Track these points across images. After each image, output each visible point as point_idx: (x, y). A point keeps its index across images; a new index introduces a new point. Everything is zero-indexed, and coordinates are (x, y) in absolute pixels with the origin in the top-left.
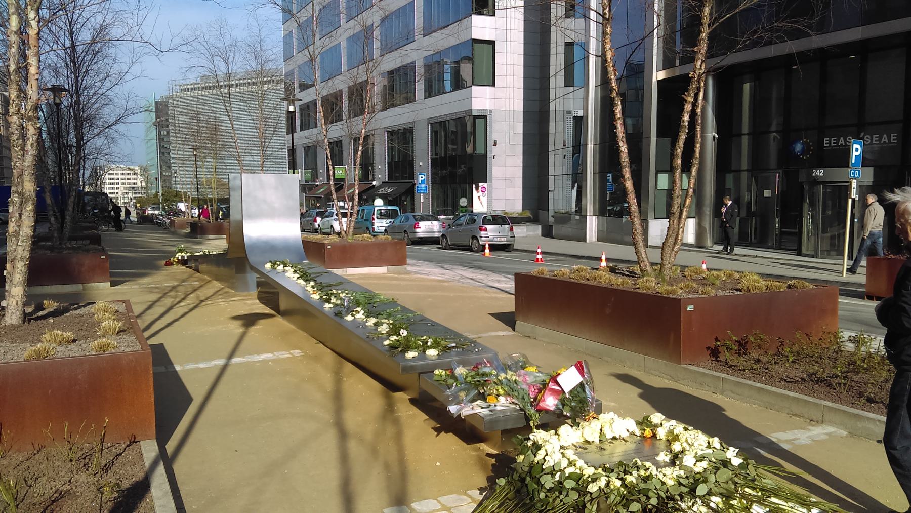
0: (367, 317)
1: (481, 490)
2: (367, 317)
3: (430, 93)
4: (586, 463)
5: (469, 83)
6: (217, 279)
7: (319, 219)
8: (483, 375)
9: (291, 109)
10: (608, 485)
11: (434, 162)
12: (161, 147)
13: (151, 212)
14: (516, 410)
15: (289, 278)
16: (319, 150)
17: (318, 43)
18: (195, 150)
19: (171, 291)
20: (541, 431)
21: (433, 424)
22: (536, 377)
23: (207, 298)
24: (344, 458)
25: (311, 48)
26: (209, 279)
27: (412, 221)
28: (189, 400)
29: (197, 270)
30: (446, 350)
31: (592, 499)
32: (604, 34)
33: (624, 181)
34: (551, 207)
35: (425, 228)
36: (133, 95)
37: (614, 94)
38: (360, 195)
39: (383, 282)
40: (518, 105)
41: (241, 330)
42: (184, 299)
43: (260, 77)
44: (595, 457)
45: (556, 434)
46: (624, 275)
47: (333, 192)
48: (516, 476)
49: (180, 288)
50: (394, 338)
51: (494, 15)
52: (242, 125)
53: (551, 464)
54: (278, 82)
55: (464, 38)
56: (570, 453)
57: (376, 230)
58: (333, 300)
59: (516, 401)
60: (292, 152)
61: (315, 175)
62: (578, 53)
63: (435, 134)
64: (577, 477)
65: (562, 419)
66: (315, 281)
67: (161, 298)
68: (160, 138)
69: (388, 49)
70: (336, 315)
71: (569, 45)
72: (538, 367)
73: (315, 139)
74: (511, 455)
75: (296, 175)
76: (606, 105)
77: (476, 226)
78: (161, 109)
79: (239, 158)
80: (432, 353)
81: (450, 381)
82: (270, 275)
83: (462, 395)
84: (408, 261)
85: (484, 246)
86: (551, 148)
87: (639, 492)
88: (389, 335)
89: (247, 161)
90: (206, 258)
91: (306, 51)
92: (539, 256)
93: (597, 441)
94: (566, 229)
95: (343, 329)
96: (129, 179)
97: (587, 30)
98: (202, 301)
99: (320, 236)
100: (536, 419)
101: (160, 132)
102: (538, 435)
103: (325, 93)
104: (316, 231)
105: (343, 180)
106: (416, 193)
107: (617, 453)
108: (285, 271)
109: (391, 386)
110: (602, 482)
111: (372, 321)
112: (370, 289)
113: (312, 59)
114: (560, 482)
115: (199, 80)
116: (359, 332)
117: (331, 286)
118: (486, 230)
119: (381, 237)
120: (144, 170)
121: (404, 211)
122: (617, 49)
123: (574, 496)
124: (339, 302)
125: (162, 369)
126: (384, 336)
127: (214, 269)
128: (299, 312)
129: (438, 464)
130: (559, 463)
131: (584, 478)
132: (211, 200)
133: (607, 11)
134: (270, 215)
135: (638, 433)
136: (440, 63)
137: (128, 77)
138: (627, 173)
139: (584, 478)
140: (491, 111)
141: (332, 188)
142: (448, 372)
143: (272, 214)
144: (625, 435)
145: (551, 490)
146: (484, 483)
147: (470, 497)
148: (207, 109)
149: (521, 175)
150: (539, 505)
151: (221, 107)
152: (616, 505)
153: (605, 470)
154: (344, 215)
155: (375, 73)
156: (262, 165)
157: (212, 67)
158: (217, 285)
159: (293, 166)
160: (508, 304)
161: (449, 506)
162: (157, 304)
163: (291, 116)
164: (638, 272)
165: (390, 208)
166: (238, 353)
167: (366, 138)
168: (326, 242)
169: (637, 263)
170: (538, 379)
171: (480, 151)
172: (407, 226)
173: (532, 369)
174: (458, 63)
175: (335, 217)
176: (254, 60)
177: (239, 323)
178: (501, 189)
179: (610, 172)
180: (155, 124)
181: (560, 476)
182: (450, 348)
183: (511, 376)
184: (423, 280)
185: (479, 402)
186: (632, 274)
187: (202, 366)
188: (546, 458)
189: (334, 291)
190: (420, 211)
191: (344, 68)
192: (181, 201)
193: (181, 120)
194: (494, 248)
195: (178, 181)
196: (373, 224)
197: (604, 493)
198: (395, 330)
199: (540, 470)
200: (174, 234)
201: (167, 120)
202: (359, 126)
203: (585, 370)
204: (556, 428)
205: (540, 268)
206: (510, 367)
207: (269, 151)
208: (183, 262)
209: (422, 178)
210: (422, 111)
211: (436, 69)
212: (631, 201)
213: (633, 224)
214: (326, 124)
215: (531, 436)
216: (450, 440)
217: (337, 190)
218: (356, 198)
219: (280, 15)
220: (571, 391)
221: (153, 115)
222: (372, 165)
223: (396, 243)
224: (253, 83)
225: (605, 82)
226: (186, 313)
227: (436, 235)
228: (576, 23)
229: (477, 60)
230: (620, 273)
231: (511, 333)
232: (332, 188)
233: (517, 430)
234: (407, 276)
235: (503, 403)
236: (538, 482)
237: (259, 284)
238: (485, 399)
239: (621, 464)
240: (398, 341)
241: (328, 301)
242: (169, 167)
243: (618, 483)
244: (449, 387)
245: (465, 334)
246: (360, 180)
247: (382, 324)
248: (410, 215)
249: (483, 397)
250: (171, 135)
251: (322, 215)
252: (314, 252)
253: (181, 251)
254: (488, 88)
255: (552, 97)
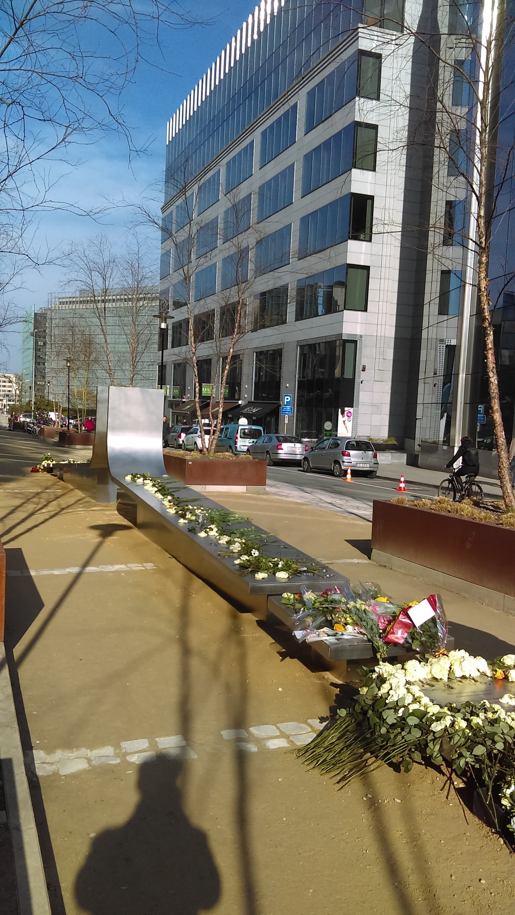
0: (220, 535)
1: (322, 720)
2: (220, 535)
3: (300, 316)
4: (432, 701)
5: (341, 307)
6: (79, 489)
7: (183, 435)
8: (332, 602)
9: (163, 326)
10: (452, 725)
11: (301, 385)
12: (37, 357)
13: (22, 419)
14: (364, 641)
15: (148, 491)
16: (188, 368)
17: (194, 263)
18: (68, 361)
19: (34, 497)
20: (387, 664)
21: (279, 648)
22: (386, 608)
23: (68, 507)
24: (185, 675)
25: (186, 268)
26: (72, 487)
27: (275, 442)
28: (40, 605)
29: (61, 478)
30: (296, 573)
31: (436, 738)
32: (480, 262)
33: (493, 412)
34: (417, 436)
35: (288, 450)
36: (13, 305)
37: (487, 324)
38: (224, 413)
39: (240, 501)
40: (390, 331)
41: (98, 540)
42: (45, 506)
43: (136, 294)
44: (443, 695)
45: (403, 668)
46: (487, 509)
47: (198, 408)
48: (358, 708)
49: (44, 495)
50: (245, 558)
51: (370, 241)
52: (115, 341)
53: (396, 699)
54: (153, 299)
55: (339, 262)
56: (416, 689)
57: (238, 449)
58: (189, 516)
59: (364, 631)
60: (162, 368)
61: (183, 393)
62: (454, 282)
63: (304, 357)
64: (421, 715)
65: (411, 653)
66: (172, 495)
67: (24, 503)
68: (37, 349)
69: (262, 270)
70: (190, 531)
71: (446, 274)
72: (390, 598)
73: (184, 356)
74: (356, 686)
75: (163, 391)
76: (479, 335)
77: (338, 450)
78: (40, 320)
79: (110, 372)
80: (282, 575)
81: (298, 606)
82: (129, 487)
83: (309, 620)
84: (268, 482)
85: (346, 472)
86: (421, 375)
87: (486, 735)
88: (240, 554)
89: (118, 374)
90: (71, 467)
91: (181, 271)
92: (402, 485)
93: (445, 678)
94: (432, 459)
95: (195, 544)
96: (4, 386)
97: (465, 258)
98: (63, 509)
99: (181, 452)
100: (383, 651)
101: (36, 343)
102: (384, 668)
103: (196, 312)
104: (180, 447)
105: (209, 398)
106: (281, 414)
107: (466, 693)
108: (144, 484)
109: (239, 606)
110: (447, 721)
111: (225, 539)
112: (227, 507)
113: (187, 278)
114: (403, 718)
115: (78, 294)
116: (211, 549)
117: (187, 501)
118: (349, 455)
119: (242, 456)
120: (19, 378)
121: (268, 431)
122: (491, 281)
123: (417, 734)
124: (194, 518)
125: (18, 573)
126: (236, 555)
127: (77, 478)
128: (155, 526)
129: (280, 689)
130: (403, 699)
131: (429, 715)
132: (80, 411)
133: (483, 240)
134: (134, 427)
135: (489, 673)
136: (313, 287)
137: (9, 287)
138: (496, 405)
139: (429, 715)
140: (361, 336)
141: (197, 405)
142: (297, 596)
143: (135, 427)
144: (476, 674)
145: (393, 726)
146: (325, 712)
147: (311, 726)
148: (83, 322)
149: (388, 401)
150: (379, 740)
151: (96, 321)
152: (459, 747)
153: (451, 709)
154: (207, 432)
155: (246, 294)
156: (132, 379)
157: (89, 281)
158: (79, 494)
159: (162, 382)
160: (365, 532)
161: (288, 733)
162: (21, 509)
163: (163, 333)
164: (503, 507)
165: (254, 427)
166: (93, 562)
167: (235, 357)
168: (188, 458)
169: (503, 498)
170: (389, 610)
171: (348, 375)
172: (270, 445)
173: (383, 600)
174: (331, 287)
175: (199, 434)
176: (131, 276)
177: (97, 532)
178: (367, 415)
179: (482, 404)
180: (32, 334)
181: (404, 712)
182: (301, 572)
183: (360, 604)
184: (282, 501)
185: (326, 629)
186: (496, 509)
187: (56, 572)
188: (391, 692)
189: (190, 507)
190: (284, 432)
191: (218, 288)
192: (52, 411)
193: (56, 331)
194: (356, 473)
195: (51, 391)
196: (236, 443)
197: (448, 733)
198: (246, 550)
199: (383, 704)
200: (44, 442)
201: (45, 331)
202: (228, 346)
203: (438, 605)
204: (403, 662)
205: (400, 497)
206: (359, 596)
207: (139, 366)
208: (49, 470)
209: (287, 399)
210: (293, 333)
211: (308, 293)
212: (499, 434)
213: (499, 456)
214: (195, 342)
215: (377, 669)
216: (294, 666)
217: (202, 408)
218: (220, 416)
219: (159, 233)
220: (422, 625)
221: (31, 326)
222: (239, 385)
223: (258, 463)
224: (130, 300)
225: (479, 313)
226: (46, 520)
227: (298, 457)
228: (453, 252)
229: (351, 286)
230: (484, 508)
231: (366, 561)
232: (197, 405)
233: (362, 662)
234: (265, 497)
235: (350, 632)
236: (380, 717)
237: (119, 496)
238: (331, 627)
239: (468, 704)
240: (249, 561)
241: (183, 516)
242: (44, 377)
243: (463, 724)
244: (297, 612)
245: (319, 559)
246: (225, 398)
247: (234, 542)
248: (273, 436)
249: (330, 624)
250: (48, 346)
251: (186, 431)
252: (174, 466)
253: (47, 459)
254: (360, 313)
255: (425, 324)
